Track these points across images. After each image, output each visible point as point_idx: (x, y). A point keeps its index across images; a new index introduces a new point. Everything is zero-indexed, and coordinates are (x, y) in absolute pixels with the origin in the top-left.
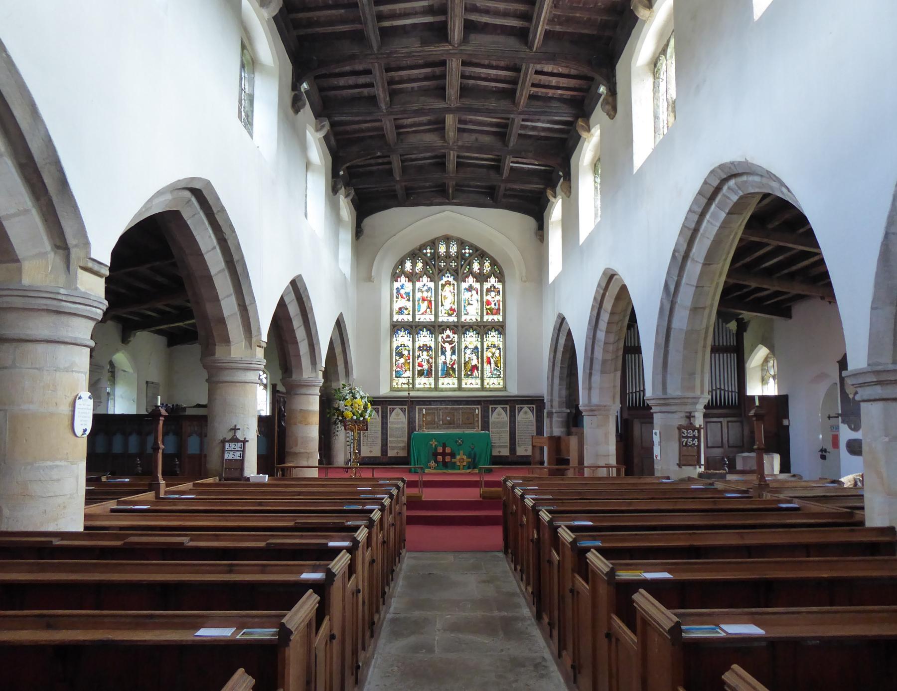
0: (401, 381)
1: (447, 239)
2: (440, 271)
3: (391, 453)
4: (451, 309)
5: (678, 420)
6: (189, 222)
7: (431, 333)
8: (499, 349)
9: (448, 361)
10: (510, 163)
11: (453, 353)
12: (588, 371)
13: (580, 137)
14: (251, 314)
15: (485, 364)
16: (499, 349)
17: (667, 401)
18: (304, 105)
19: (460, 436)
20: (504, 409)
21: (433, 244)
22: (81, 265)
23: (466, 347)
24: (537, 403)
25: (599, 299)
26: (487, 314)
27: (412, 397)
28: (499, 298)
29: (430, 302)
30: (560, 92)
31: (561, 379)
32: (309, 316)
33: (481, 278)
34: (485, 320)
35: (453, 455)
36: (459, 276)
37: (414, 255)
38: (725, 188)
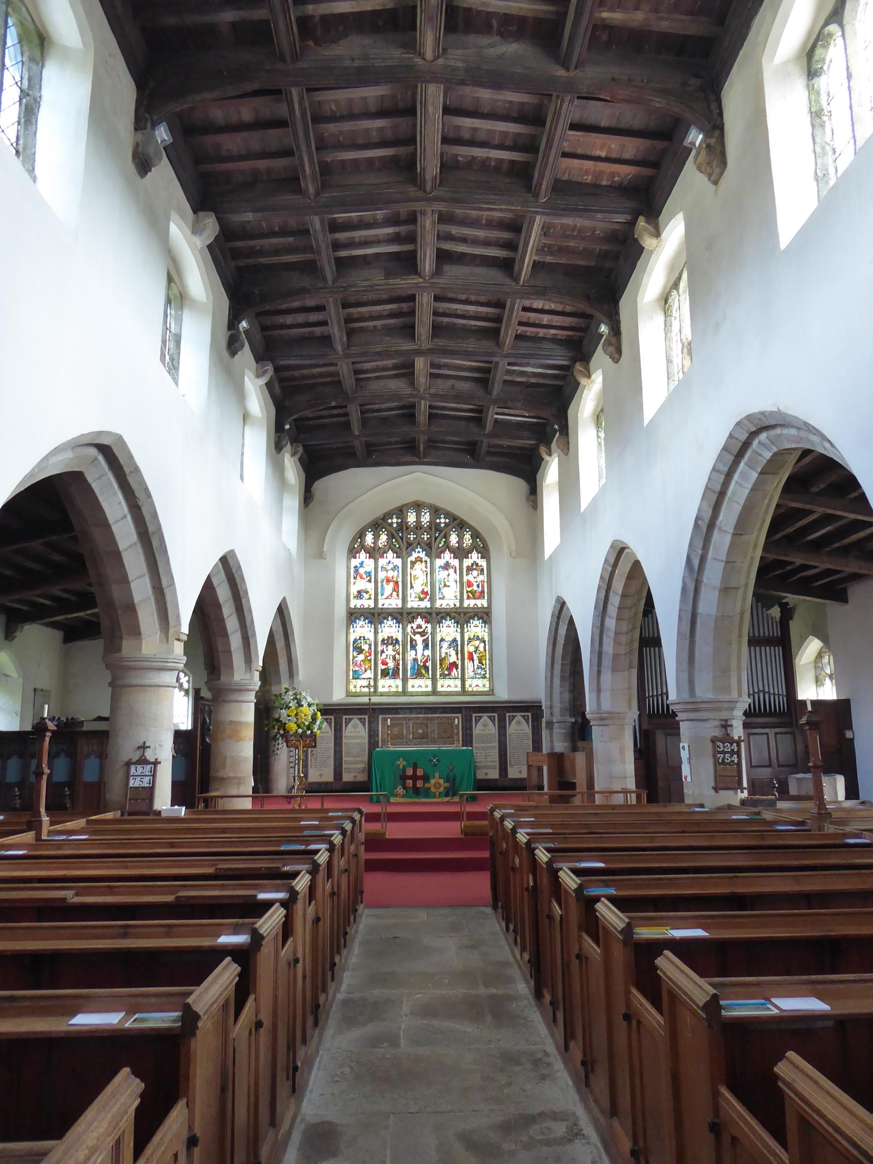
1: (418, 506)
2: (409, 544)
4: (423, 592)
5: (711, 730)
7: (398, 622)
9: (419, 657)
10: (494, 414)
11: (426, 647)
12: (595, 669)
13: (579, 384)
15: (466, 661)
16: (484, 642)
19: (435, 754)
20: (492, 719)
21: (401, 512)
24: (532, 710)
26: (468, 597)
28: (484, 577)
29: (397, 583)
30: (553, 331)
31: (563, 678)
32: (243, 601)
34: (465, 605)
35: (426, 778)
37: (377, 526)
38: (755, 443)
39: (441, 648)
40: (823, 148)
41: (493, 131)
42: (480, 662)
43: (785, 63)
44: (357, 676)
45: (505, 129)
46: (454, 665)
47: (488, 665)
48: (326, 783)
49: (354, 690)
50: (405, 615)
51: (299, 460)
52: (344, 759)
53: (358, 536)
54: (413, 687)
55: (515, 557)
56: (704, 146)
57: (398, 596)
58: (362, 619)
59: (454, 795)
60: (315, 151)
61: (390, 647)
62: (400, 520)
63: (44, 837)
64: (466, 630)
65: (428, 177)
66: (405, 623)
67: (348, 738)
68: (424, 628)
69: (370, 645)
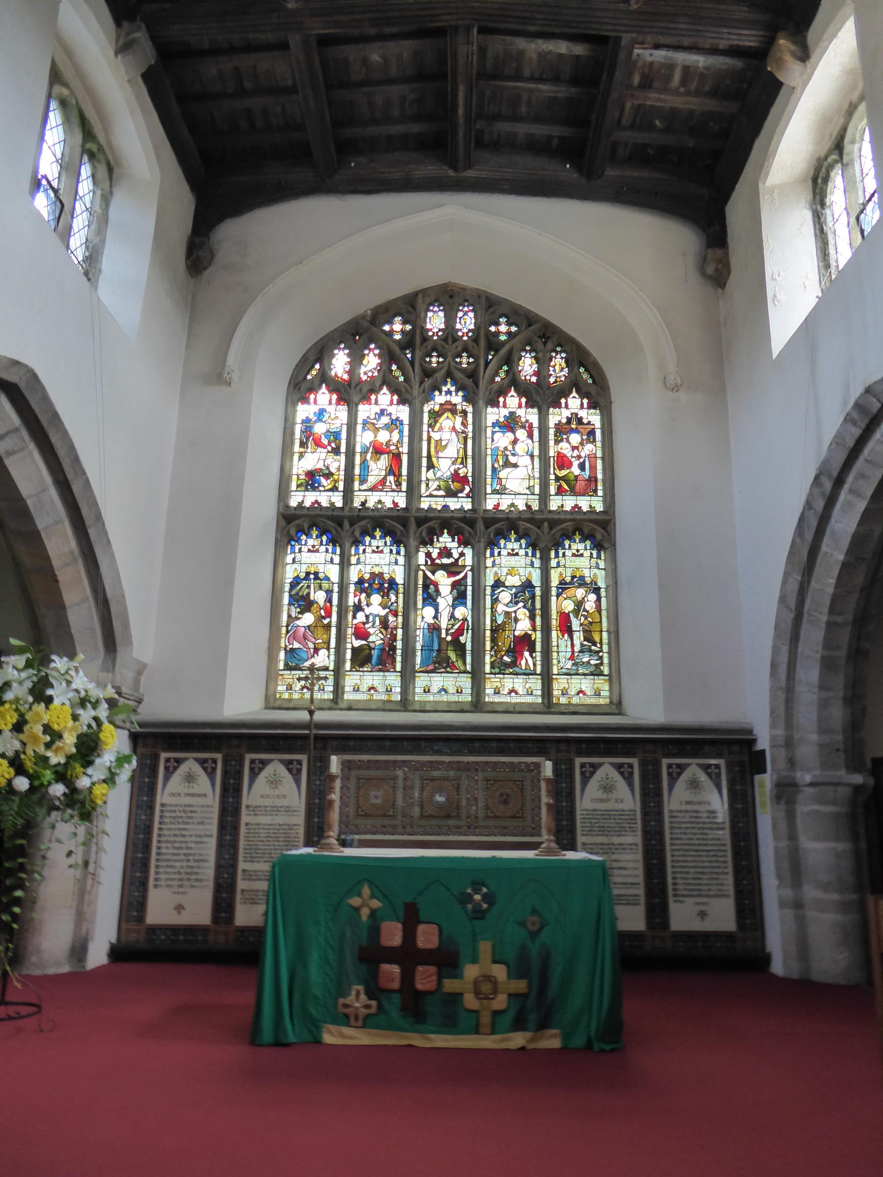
1: (450, 297)
2: (428, 373)
4: (456, 477)
7: (397, 542)
8: (597, 591)
9: (444, 623)
11: (460, 598)
16: (597, 591)
19: (478, 875)
20: (625, 772)
21: (411, 306)
23: (498, 584)
24: (735, 753)
26: (560, 491)
29: (397, 457)
31: (828, 665)
33: (542, 396)
35: (447, 960)
37: (358, 333)
42: (588, 637)
46: (525, 642)
47: (606, 648)
48: (190, 930)
50: (413, 526)
52: (242, 865)
53: (312, 358)
55: (676, 388)
57: (399, 484)
58: (315, 533)
59: (543, 1025)
62: (408, 327)
64: (553, 563)
66: (413, 543)
67: (255, 810)
68: (456, 555)
69: (329, 592)
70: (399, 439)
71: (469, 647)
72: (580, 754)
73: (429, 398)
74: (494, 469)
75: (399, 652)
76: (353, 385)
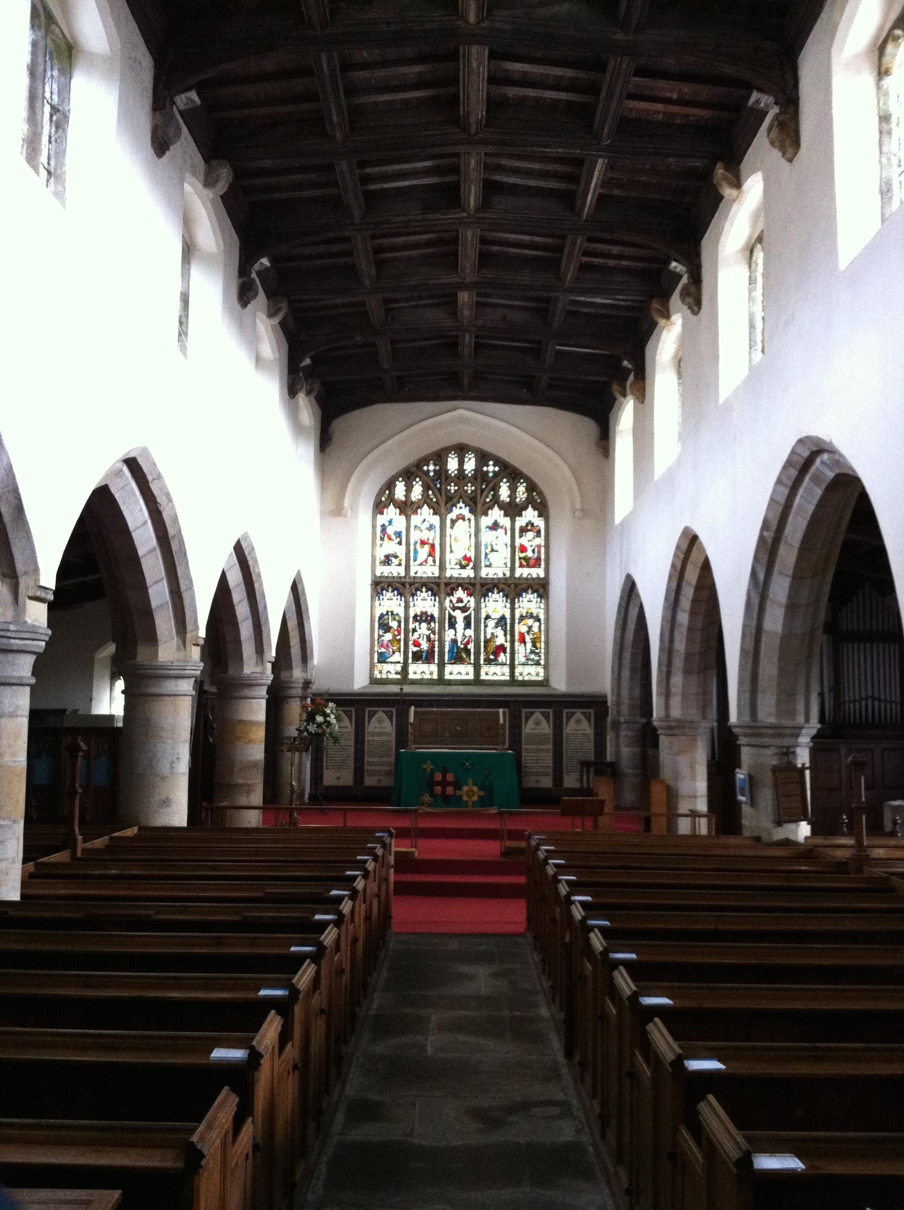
0: (386, 667)
1: (461, 450)
3: (369, 781)
5: (770, 758)
6: (117, 496)
9: (459, 639)
11: (467, 625)
12: (664, 669)
14: (186, 602)
15: (517, 644)
16: (539, 620)
17: (754, 731)
18: (256, 295)
20: (546, 716)
22: (30, 594)
23: (488, 617)
24: (594, 705)
25: (679, 566)
26: (521, 566)
27: (406, 695)
28: (540, 541)
29: (433, 547)
30: (624, 263)
32: (256, 585)
33: (513, 510)
34: (517, 575)
35: (457, 785)
36: (478, 507)
37: (409, 475)
38: (818, 461)
39: (486, 626)
40: (889, 159)
41: (549, 75)
42: (534, 645)
43: (857, 56)
44: (383, 659)
45: (560, 73)
46: (502, 648)
49: (379, 676)
51: (316, 398)
52: (366, 759)
54: (451, 674)
56: (776, 123)
57: (434, 561)
60: (342, 95)
61: (424, 625)
62: (438, 468)
63: (79, 854)
64: (517, 605)
65: (473, 120)
66: (443, 596)
67: (373, 734)
69: (399, 622)
70: (434, 536)
71: (472, 651)
72: (525, 707)
73: (451, 511)
74: (486, 554)
75: (436, 654)
76: (408, 504)
